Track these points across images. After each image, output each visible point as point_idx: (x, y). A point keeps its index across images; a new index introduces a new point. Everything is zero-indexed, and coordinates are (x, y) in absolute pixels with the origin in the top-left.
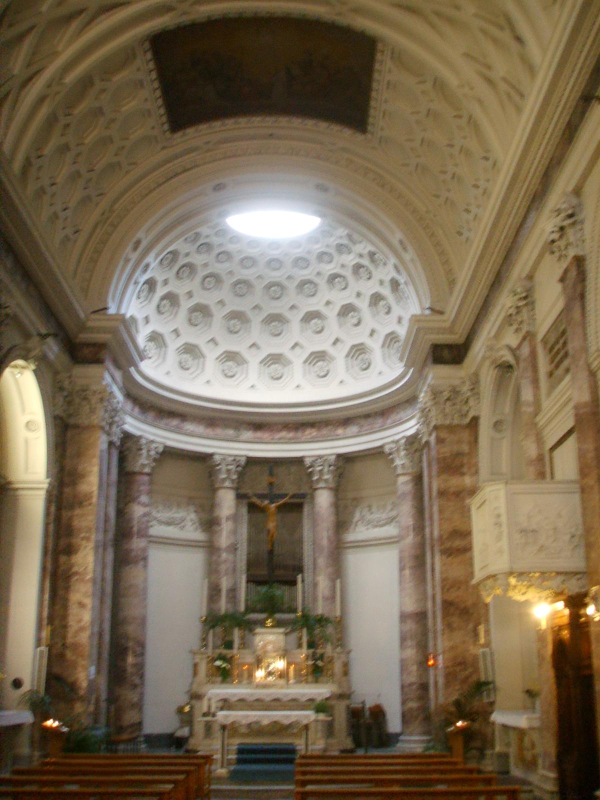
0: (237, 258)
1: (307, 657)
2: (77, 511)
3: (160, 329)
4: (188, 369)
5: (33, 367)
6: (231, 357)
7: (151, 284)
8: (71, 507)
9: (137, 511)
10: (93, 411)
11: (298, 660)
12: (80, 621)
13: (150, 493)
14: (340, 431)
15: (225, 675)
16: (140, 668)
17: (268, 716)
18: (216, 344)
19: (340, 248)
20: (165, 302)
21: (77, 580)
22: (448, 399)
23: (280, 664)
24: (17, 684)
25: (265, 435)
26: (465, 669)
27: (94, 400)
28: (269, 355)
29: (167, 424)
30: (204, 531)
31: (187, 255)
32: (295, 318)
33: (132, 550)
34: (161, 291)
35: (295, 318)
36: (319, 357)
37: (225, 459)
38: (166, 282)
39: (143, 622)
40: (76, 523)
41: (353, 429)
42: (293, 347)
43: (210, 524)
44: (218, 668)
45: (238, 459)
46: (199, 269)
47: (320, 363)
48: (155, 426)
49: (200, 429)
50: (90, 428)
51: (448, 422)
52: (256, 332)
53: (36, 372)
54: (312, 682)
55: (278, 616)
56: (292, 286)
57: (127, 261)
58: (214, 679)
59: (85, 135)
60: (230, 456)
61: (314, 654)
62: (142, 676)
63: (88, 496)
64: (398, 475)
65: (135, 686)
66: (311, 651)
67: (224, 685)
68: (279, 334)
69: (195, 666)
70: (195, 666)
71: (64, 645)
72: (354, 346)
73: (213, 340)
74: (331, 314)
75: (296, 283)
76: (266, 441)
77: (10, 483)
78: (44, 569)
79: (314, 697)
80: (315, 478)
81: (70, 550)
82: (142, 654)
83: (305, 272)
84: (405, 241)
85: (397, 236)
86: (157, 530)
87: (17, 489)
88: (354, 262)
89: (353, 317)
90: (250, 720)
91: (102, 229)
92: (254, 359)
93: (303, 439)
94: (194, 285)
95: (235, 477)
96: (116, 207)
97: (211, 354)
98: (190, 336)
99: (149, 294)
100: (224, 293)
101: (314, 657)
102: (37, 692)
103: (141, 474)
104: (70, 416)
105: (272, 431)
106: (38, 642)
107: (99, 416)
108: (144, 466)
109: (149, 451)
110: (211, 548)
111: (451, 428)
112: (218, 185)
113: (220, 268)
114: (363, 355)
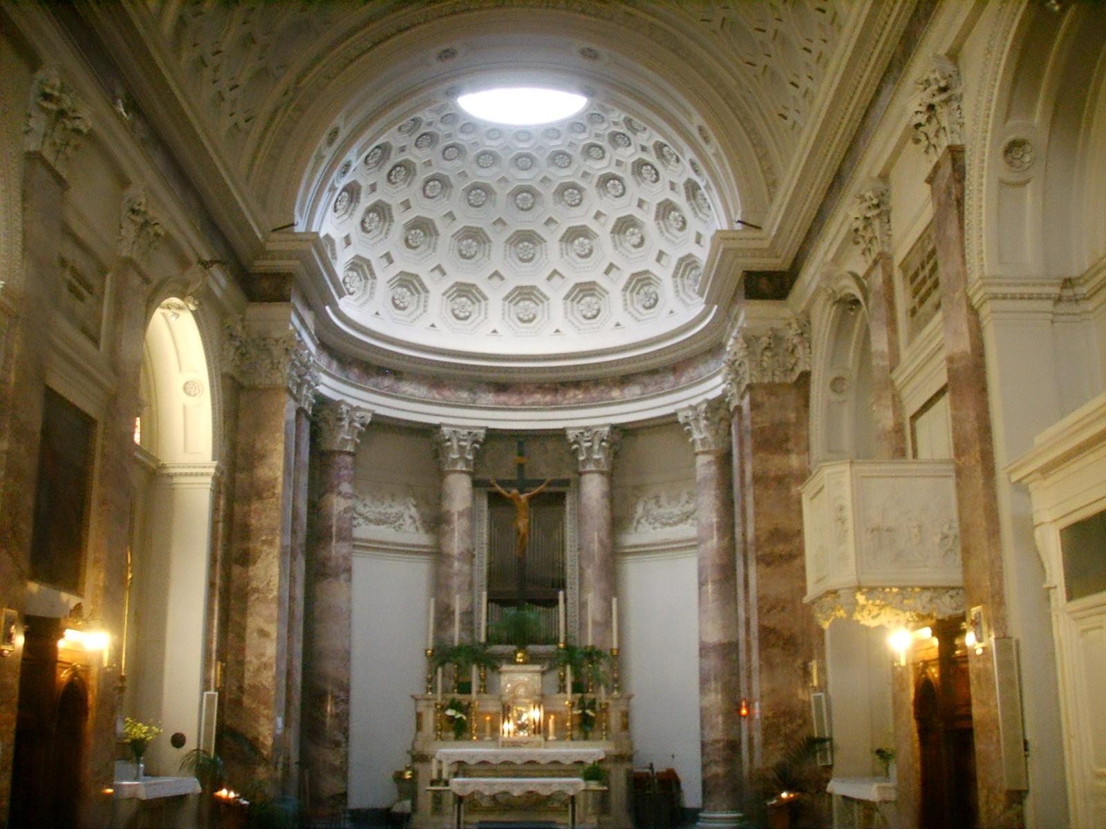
0: (472, 154)
2: (256, 505)
4: (404, 309)
7: (353, 192)
8: (247, 499)
9: (337, 505)
10: (275, 366)
14: (616, 393)
15: (460, 729)
16: (343, 719)
19: (614, 138)
24: (178, 741)
25: (513, 399)
26: (791, 721)
27: (277, 351)
30: (427, 532)
31: (403, 149)
32: (552, 238)
39: (346, 657)
41: (635, 390)
43: (436, 522)
44: (452, 719)
47: (588, 299)
49: (422, 391)
51: (766, 380)
53: (195, 314)
54: (578, 739)
55: (531, 648)
58: (444, 734)
61: (582, 700)
62: (346, 731)
63: (271, 484)
64: (696, 454)
66: (579, 695)
67: (458, 743)
69: (419, 716)
70: (419, 716)
71: (241, 688)
74: (603, 231)
77: (163, 467)
81: (246, 559)
86: (363, 531)
87: (171, 476)
89: (633, 234)
94: (412, 191)
97: (437, 288)
100: (455, 202)
101: (582, 705)
105: (521, 393)
106: (206, 684)
110: (439, 556)
111: (771, 389)
112: (447, 51)
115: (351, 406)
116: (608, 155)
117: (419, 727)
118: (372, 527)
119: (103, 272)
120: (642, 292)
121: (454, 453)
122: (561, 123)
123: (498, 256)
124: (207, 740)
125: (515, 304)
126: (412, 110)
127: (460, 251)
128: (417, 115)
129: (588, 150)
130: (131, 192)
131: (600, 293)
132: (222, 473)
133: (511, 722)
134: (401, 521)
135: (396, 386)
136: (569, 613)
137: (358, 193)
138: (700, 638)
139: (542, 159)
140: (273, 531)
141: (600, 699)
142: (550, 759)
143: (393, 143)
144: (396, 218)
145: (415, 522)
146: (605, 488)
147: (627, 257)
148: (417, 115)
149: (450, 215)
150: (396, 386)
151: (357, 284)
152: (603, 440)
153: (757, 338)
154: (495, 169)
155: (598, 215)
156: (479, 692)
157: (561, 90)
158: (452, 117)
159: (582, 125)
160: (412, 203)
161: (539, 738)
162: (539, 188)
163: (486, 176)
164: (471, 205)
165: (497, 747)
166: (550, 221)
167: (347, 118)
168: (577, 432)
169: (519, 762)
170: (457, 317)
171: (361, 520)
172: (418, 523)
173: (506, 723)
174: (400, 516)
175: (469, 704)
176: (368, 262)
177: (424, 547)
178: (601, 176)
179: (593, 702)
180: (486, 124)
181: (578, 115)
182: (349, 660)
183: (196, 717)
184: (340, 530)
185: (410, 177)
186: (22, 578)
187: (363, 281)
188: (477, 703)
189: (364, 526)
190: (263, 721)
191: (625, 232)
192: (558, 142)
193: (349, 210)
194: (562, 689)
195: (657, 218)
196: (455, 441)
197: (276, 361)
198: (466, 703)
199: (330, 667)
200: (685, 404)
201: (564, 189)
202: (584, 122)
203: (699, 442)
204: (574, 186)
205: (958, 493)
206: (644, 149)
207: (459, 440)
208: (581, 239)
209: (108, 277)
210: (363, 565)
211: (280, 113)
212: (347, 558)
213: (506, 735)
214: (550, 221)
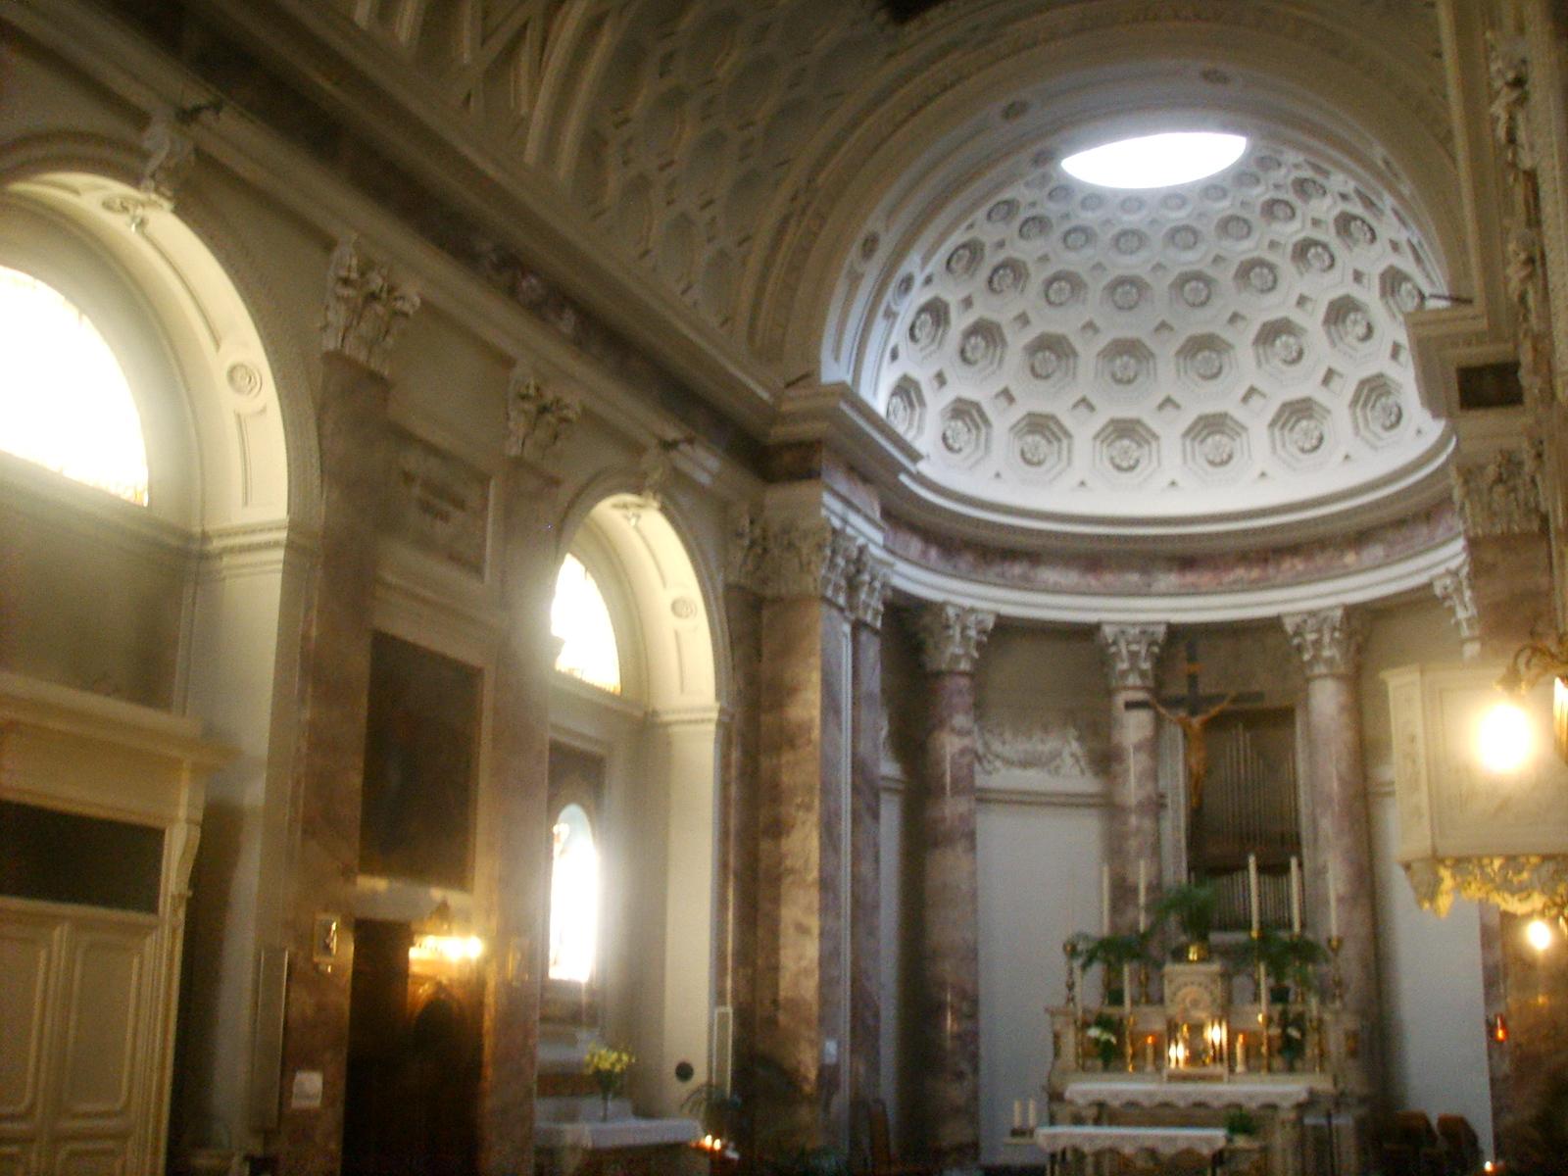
0: (1106, 236)
1: (1269, 1020)
2: (787, 757)
3: (970, 393)
4: (1039, 463)
5: (656, 504)
6: (1125, 430)
7: (936, 311)
8: (776, 748)
9: (950, 745)
10: (805, 567)
11: (1252, 1027)
12: (801, 958)
13: (980, 709)
14: (1350, 558)
15: (1108, 1058)
16: (969, 1040)
17: (1135, 1138)
18: (1091, 408)
19: (1302, 187)
20: (973, 340)
21: (793, 883)
22: (1500, 480)
23: (1216, 1034)
24: (684, 1072)
25: (1203, 578)
27: (805, 549)
28: (1201, 418)
29: (1002, 575)
30: (1096, 774)
31: (1001, 244)
32: (1242, 340)
33: (943, 819)
34: (960, 322)
35: (1242, 340)
36: (1298, 411)
37: (1123, 632)
38: (968, 303)
39: (972, 955)
40: (786, 779)
41: (1376, 551)
42: (1245, 399)
43: (1105, 760)
44: (1097, 1041)
45: (1151, 629)
46: (1031, 268)
47: (1304, 423)
48: (972, 580)
49: (1071, 577)
50: (802, 600)
51: (1498, 530)
52: (1166, 375)
53: (663, 510)
54: (1280, 1071)
55: (1215, 937)
56: (1225, 276)
57: (855, 279)
58: (1089, 1063)
59: (512, 105)
60: (1134, 624)
61: (1284, 1014)
62: (974, 1058)
63: (804, 728)
64: (1463, 642)
65: (960, 1076)
66: (1279, 1007)
67: (1106, 1076)
68: (1215, 376)
69: (1057, 1037)
70: (1057, 1037)
71: (775, 1002)
72: (1363, 383)
73: (1084, 401)
74: (1312, 321)
75: (1171, 278)
76: (1204, 589)
77: (655, 713)
78: (723, 866)
79: (1277, 1101)
80: (1306, 657)
81: (778, 829)
82: (973, 1016)
83: (1246, 246)
84: (1392, 160)
85: (1378, 152)
86: (1000, 778)
87: (668, 724)
88: (1336, 212)
89: (1355, 322)
90: (1099, 1145)
91: (798, 226)
92: (1170, 430)
93: (1280, 579)
94: (1030, 298)
95: (1146, 666)
96: (820, 180)
97: (1084, 430)
98: (1033, 399)
99: (937, 330)
100: (1093, 306)
101: (1285, 1022)
102: (720, 1086)
103: (953, 673)
104: (764, 581)
105: (1216, 568)
106: (719, 997)
107: (823, 575)
108: (956, 658)
109: (964, 628)
110: (1109, 807)
112: (1012, 105)
113: (1073, 261)
114: (1383, 400)
115: (963, 608)
116: (1299, 213)
117: (1057, 1054)
118: (1017, 772)
119: (483, 480)
120: (1378, 405)
121: (1123, 661)
122: (1224, 174)
123: (1244, 361)
124: (721, 1070)
125: (1292, 429)
126: (999, 187)
127: (1113, 376)
128: (1007, 194)
129: (1270, 208)
130: (518, 372)
131: (1232, 429)
132: (732, 717)
133: (1181, 1046)
134: (1058, 762)
135: (1032, 574)
136: (1306, 883)
137: (946, 312)
138: (1481, 918)
139: (1208, 229)
140: (810, 790)
141: (1310, 1011)
142: (1261, 1100)
143: (984, 239)
144: (1009, 338)
145: (1077, 761)
146: (1343, 698)
147: (1351, 357)
148: (1007, 194)
149: (1090, 326)
150: (1032, 574)
151: (964, 437)
152: (1334, 629)
153: (1481, 468)
154: (1143, 254)
155: (1302, 301)
156: (1135, 1002)
157: (1125, 138)
158: (1065, 190)
159: (1251, 175)
160: (1032, 315)
161: (1220, 1069)
162: (1210, 272)
163: (1132, 264)
164: (1120, 308)
165: (1161, 1081)
166: (1235, 318)
167: (891, 214)
168: (1298, 619)
169: (1182, 1104)
170: (1119, 468)
171: (998, 763)
172: (1082, 763)
173: (1173, 1047)
174: (1056, 755)
175: (1121, 1020)
176: (977, 406)
177: (1092, 796)
178: (1295, 245)
179: (1301, 1016)
180: (1115, 193)
181: (1242, 162)
182: (975, 958)
183: (705, 1036)
184: (955, 781)
185: (1022, 283)
186: (347, 874)
187: (974, 431)
188: (1132, 1020)
189: (1003, 771)
190: (804, 1045)
191: (1344, 321)
192: (1225, 204)
193: (937, 339)
194: (1256, 998)
195: (1383, 294)
196: (1123, 645)
197: (805, 561)
198: (1117, 1018)
199: (947, 969)
200: (1441, 569)
201: (1246, 270)
202: (1254, 169)
203: (1465, 625)
204: (1260, 263)
205: (723, 776)
206: (1344, 197)
207: (1128, 643)
208: (1284, 338)
209: (492, 483)
210: (997, 830)
211: (793, 222)
212: (966, 819)
213: (1173, 1065)
214: (1235, 318)
